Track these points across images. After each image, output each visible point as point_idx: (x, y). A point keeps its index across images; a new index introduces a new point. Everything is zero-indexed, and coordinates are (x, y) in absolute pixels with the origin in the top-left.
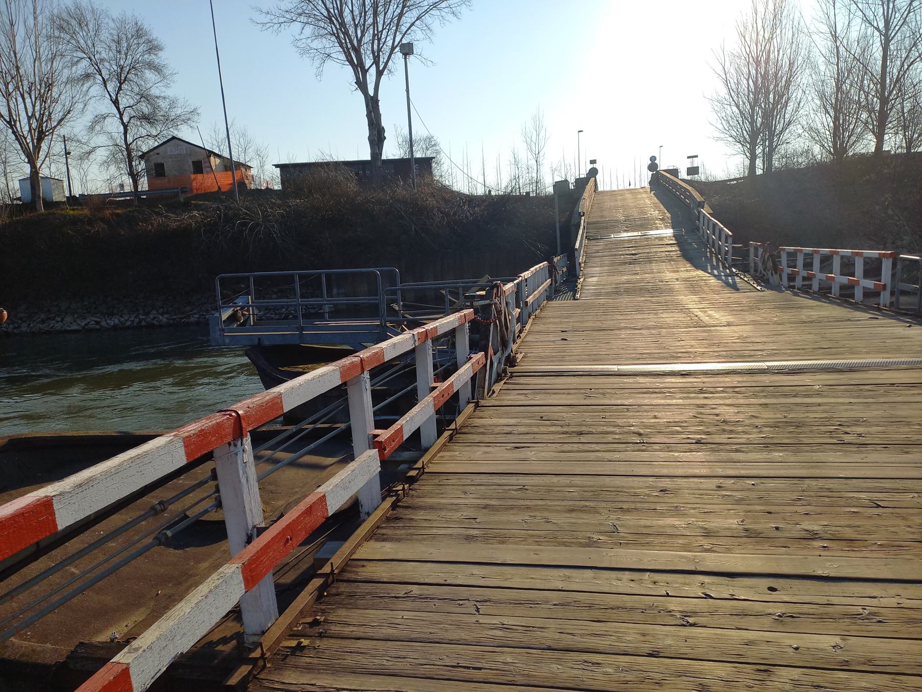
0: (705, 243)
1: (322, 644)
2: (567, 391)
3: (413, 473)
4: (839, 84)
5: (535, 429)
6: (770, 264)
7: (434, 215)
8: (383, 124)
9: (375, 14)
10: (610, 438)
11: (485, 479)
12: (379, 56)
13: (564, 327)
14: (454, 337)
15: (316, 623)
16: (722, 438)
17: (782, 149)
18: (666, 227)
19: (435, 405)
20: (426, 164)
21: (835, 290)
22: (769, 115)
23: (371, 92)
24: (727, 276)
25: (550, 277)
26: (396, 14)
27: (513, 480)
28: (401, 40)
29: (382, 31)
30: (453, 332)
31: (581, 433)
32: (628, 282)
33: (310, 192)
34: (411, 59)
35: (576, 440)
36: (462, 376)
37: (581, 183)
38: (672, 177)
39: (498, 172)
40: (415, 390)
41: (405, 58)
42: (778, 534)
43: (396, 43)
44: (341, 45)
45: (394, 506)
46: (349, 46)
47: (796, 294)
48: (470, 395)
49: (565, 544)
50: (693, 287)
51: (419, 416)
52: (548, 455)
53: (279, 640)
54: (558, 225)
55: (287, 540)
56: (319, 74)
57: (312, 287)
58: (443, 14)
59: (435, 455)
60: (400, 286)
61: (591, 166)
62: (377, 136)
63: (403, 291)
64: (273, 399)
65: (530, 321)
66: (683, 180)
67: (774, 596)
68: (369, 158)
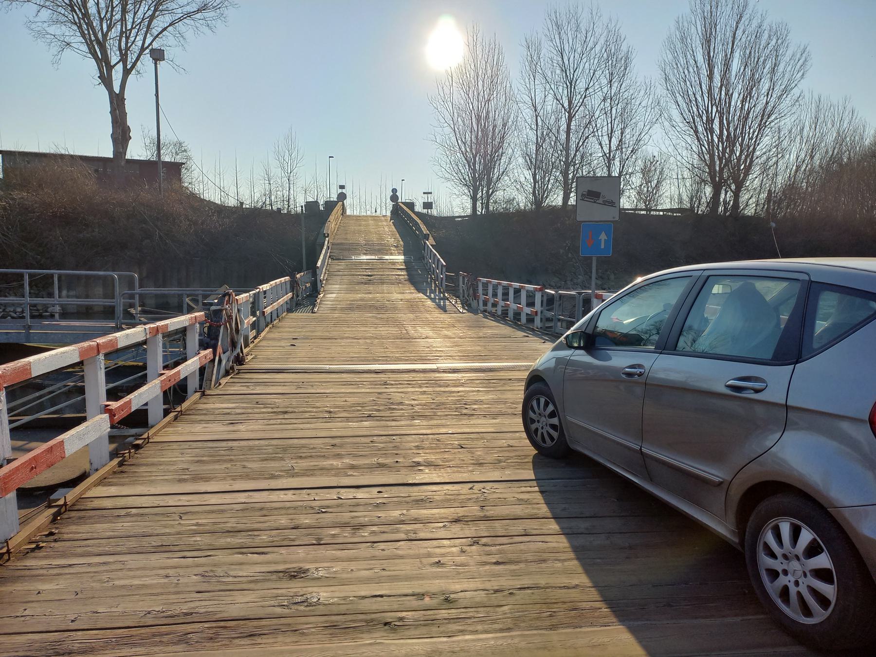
0: (428, 270)
1: (57, 545)
2: (283, 384)
3: (139, 442)
4: (538, 146)
5: (250, 411)
6: (471, 291)
7: (181, 222)
8: (128, 124)
9: (124, 11)
10: (307, 415)
11: (200, 444)
12: (126, 54)
13: (296, 335)
14: (185, 335)
15: (51, 534)
16: (387, 413)
17: (499, 195)
18: (399, 254)
19: (162, 387)
20: (175, 168)
21: (511, 314)
22: (489, 167)
23: (117, 89)
24: (440, 299)
25: (292, 291)
26: (147, 15)
27: (224, 444)
28: (151, 44)
29: (131, 30)
30: (183, 331)
31: (286, 412)
32: (362, 300)
33: (40, 186)
34: (162, 65)
35: (281, 417)
36: (190, 366)
37: (330, 205)
38: (407, 210)
39: (252, 186)
40: (146, 375)
41: (156, 64)
42: (397, 465)
43: (146, 45)
44: (83, 35)
45: (121, 464)
46: (93, 38)
47: (485, 317)
48: (198, 387)
49: (253, 479)
50: (412, 307)
51: (148, 394)
52: (256, 427)
53: (20, 545)
54: (304, 243)
55: (32, 468)
56: (56, 62)
57: (42, 286)
58: (198, 25)
59: (160, 430)
60: (138, 290)
61: (340, 191)
62: (121, 134)
63: (141, 295)
64: (24, 366)
65: (267, 329)
66: (418, 214)
67: (380, 495)
68: (112, 156)
